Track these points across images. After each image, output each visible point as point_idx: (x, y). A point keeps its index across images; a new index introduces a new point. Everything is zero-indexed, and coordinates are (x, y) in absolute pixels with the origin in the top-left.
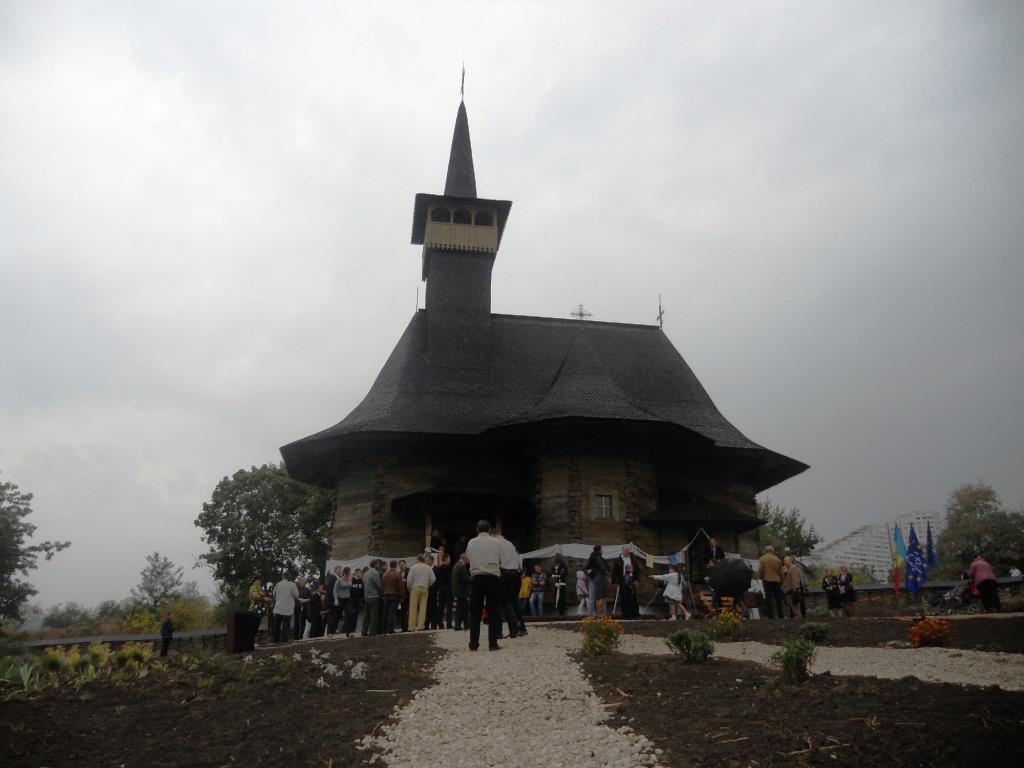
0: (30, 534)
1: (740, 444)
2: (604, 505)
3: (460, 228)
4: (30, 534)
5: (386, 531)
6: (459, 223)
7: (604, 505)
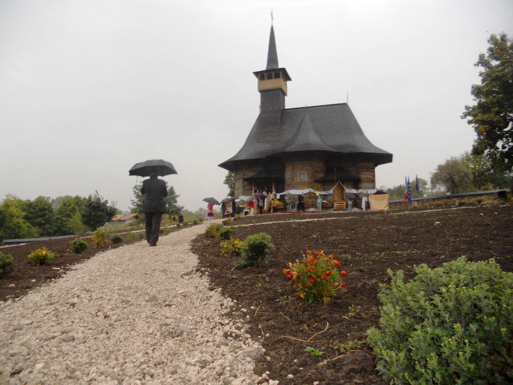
0: (107, 203)
1: (385, 153)
2: (304, 176)
3: (269, 81)
4: (107, 203)
5: (246, 188)
6: (273, 76)
7: (304, 176)
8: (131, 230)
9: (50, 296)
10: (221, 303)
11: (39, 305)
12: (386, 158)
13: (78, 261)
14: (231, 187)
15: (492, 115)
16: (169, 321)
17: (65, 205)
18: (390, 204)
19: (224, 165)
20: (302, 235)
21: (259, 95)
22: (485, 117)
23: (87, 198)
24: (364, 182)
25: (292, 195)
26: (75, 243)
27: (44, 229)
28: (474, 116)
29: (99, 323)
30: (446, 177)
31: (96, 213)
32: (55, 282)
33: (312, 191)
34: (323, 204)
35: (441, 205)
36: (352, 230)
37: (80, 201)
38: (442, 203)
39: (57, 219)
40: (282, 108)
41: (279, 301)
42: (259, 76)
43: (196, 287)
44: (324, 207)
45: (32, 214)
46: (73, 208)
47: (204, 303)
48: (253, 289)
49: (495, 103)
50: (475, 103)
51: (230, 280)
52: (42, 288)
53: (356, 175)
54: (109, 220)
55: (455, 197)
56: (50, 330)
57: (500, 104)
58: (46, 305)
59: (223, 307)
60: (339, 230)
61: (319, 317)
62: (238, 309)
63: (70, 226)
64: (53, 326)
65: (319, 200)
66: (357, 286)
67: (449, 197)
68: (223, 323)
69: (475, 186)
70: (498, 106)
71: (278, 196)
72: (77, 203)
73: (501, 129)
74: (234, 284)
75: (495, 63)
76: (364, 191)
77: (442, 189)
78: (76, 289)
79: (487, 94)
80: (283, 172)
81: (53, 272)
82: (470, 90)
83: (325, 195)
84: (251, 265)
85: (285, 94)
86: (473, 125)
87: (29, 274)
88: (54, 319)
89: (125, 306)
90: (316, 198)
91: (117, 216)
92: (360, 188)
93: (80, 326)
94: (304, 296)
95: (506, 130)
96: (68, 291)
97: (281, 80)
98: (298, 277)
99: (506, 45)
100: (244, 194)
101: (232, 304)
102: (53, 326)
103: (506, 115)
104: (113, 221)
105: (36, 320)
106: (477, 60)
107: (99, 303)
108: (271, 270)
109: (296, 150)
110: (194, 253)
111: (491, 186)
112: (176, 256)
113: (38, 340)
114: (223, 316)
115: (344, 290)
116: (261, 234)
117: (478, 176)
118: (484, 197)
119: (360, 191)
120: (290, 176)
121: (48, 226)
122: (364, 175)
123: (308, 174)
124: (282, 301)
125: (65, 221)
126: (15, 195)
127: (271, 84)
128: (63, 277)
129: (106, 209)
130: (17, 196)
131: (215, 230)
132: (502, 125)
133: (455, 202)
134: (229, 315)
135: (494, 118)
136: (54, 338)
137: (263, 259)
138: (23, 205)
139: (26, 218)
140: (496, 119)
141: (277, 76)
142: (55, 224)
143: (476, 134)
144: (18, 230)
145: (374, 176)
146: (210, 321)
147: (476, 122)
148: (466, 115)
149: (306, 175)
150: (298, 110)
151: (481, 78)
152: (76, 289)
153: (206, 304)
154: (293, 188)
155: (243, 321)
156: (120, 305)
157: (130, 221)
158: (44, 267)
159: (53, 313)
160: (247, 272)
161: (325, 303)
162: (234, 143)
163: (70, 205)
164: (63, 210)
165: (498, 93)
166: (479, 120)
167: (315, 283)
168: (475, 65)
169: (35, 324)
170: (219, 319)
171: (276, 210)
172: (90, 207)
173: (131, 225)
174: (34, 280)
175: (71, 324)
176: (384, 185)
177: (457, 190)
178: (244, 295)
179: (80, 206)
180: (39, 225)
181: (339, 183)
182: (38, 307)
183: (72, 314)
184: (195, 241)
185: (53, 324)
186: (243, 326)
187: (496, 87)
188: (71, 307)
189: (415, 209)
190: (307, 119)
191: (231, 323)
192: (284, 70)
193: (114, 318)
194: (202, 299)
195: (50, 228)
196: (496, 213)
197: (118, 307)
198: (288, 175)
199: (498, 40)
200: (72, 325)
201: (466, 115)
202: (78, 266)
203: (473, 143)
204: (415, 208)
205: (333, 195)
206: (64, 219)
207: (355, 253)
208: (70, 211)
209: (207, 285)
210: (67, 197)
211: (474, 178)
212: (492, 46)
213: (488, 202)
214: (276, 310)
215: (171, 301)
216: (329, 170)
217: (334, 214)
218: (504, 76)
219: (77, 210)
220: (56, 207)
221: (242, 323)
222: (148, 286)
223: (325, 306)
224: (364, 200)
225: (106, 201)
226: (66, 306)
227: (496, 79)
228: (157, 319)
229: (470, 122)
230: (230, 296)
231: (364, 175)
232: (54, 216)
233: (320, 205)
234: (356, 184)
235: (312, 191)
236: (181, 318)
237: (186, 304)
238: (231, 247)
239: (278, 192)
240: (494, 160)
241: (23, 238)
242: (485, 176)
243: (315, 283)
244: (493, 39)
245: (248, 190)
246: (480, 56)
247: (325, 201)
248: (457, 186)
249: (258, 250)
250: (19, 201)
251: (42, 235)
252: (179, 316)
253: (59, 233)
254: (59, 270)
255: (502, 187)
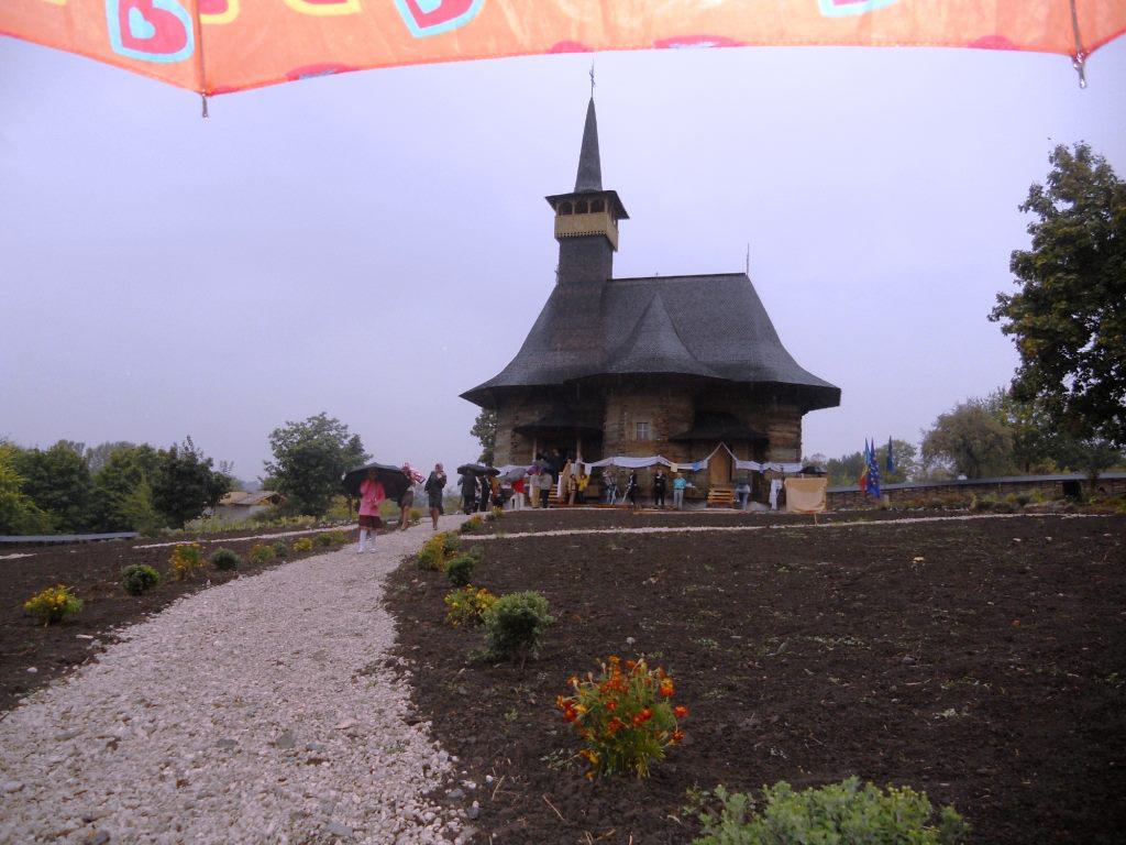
0: (212, 465)
2: (648, 431)
3: (579, 217)
4: (212, 465)
5: (519, 449)
6: (589, 208)
8: (261, 531)
9: (65, 715)
10: (425, 761)
11: (40, 736)
12: (827, 396)
13: (137, 615)
14: (485, 442)
15: (1054, 317)
16: (312, 805)
17: (116, 463)
18: (830, 495)
19: (472, 396)
20: (628, 576)
21: (555, 247)
22: (1039, 321)
23: (168, 450)
24: (777, 446)
25: (618, 468)
26: (132, 573)
27: (66, 515)
28: (1016, 317)
29: (164, 797)
30: (954, 441)
31: (185, 485)
32: (80, 675)
33: (664, 461)
34: (686, 490)
35: (939, 506)
36: (736, 567)
37: (151, 457)
38: (943, 501)
39: (97, 494)
40: (605, 277)
41: (547, 762)
42: (558, 205)
43: (381, 712)
44: (690, 498)
45: (40, 482)
46: (135, 474)
47: (391, 759)
48: (496, 727)
49: (1060, 293)
50: (1019, 289)
51: (452, 699)
52: (50, 691)
53: (760, 431)
54: (213, 503)
55: (973, 486)
56: (59, 810)
57: (1070, 294)
58: (56, 739)
59: (429, 774)
60: (708, 568)
61: (623, 813)
62: (457, 784)
63: (125, 511)
64: (65, 799)
65: (680, 483)
66: (714, 731)
67: (962, 486)
68: (422, 817)
69: (1019, 466)
70: (1066, 300)
71: (588, 468)
72: (143, 462)
73: (1072, 348)
74: (460, 710)
75: (1062, 206)
76: (776, 467)
77: (946, 465)
78: (123, 698)
79: (1046, 271)
80: (601, 417)
81: (77, 645)
82: (1008, 261)
83: (690, 472)
84: (505, 659)
85: (612, 247)
86: (1014, 335)
87: (25, 649)
88: (71, 780)
89: (223, 756)
90: (673, 476)
91: (232, 494)
92: (768, 461)
93: (123, 805)
94: (598, 757)
95: (1081, 350)
96: (105, 703)
97: (606, 216)
98: (587, 717)
99: (1087, 170)
100: (513, 461)
101: (446, 767)
102: (65, 799)
103: (1082, 318)
104: (223, 505)
105: (32, 781)
106: (1024, 196)
107: (170, 741)
108: (542, 676)
109: (632, 371)
110: (388, 609)
111: (1051, 464)
112: (350, 615)
113: (33, 837)
114: (423, 796)
115: (687, 739)
116: (527, 593)
117: (1025, 442)
118: (1032, 492)
119: (766, 466)
120: (616, 426)
121: (75, 508)
122: (778, 432)
123: (656, 425)
124: (553, 761)
125: (113, 500)
126: (7, 438)
127: (583, 224)
128: (98, 662)
129: (209, 478)
130: (11, 439)
131: (441, 555)
132: (1074, 339)
133: (970, 499)
134: (437, 797)
135: (1057, 325)
136: (65, 833)
137: (530, 648)
138: (23, 459)
139: (28, 490)
140: (1061, 326)
141: (597, 208)
142: (93, 505)
143: (1019, 355)
144: (6, 515)
145: (799, 435)
146: (395, 811)
147: (1019, 331)
148: (998, 314)
149: (651, 428)
150: (640, 282)
151: (1032, 237)
152: (123, 698)
153: (394, 763)
154: (623, 453)
155: (465, 815)
156: (213, 752)
157: (261, 508)
158: (58, 628)
159: (68, 762)
160: (492, 675)
161: (639, 777)
162: (497, 340)
163: (128, 464)
164: (110, 475)
165: (1068, 272)
166: (1025, 327)
167: (621, 733)
168: (1021, 208)
169: (30, 793)
170: (416, 808)
171: (581, 499)
172: (171, 473)
173: (260, 517)
174: (33, 669)
175: (105, 798)
176: (820, 452)
177: (979, 471)
178: (477, 743)
179: (149, 468)
180: (55, 506)
181: (722, 446)
182: (37, 744)
183: (109, 769)
184: (395, 578)
185: (66, 793)
186: (461, 830)
187: (1062, 258)
188: (110, 749)
189: (883, 513)
190: (658, 303)
191: (438, 822)
192: (613, 195)
193: (197, 786)
194: (389, 747)
195: (78, 514)
196: (1049, 538)
197: (207, 758)
198: (611, 425)
199: (1072, 159)
200: (106, 801)
201: (998, 314)
202: (133, 630)
203: (1013, 375)
204: (884, 509)
205: (707, 472)
206: (112, 494)
207: (728, 637)
208: (127, 477)
209: (403, 706)
210: (123, 445)
211: (1017, 445)
212: (1059, 170)
213: (1042, 504)
214: (537, 787)
215: (322, 748)
216: (701, 418)
217: (707, 515)
218: (1082, 235)
219: (144, 476)
220: (96, 467)
221: (463, 821)
222: (279, 701)
223: (640, 783)
224: (775, 485)
225: (210, 462)
226: (98, 745)
227: (1066, 240)
228: (287, 797)
229: (1006, 330)
230: (446, 747)
231: (778, 432)
232: (90, 487)
233: (681, 492)
234: (760, 450)
235: (664, 461)
236: (337, 799)
237: (354, 757)
238: (467, 606)
239: (587, 460)
240: (1057, 414)
241: (17, 535)
242: (1041, 442)
243: (621, 733)
244: (1060, 155)
245: (522, 453)
246: (1032, 190)
247: (690, 485)
248: (977, 462)
249: (518, 628)
250: (16, 451)
251: (60, 529)
252: (333, 793)
253: (99, 526)
254: (89, 641)
255: (1076, 467)
